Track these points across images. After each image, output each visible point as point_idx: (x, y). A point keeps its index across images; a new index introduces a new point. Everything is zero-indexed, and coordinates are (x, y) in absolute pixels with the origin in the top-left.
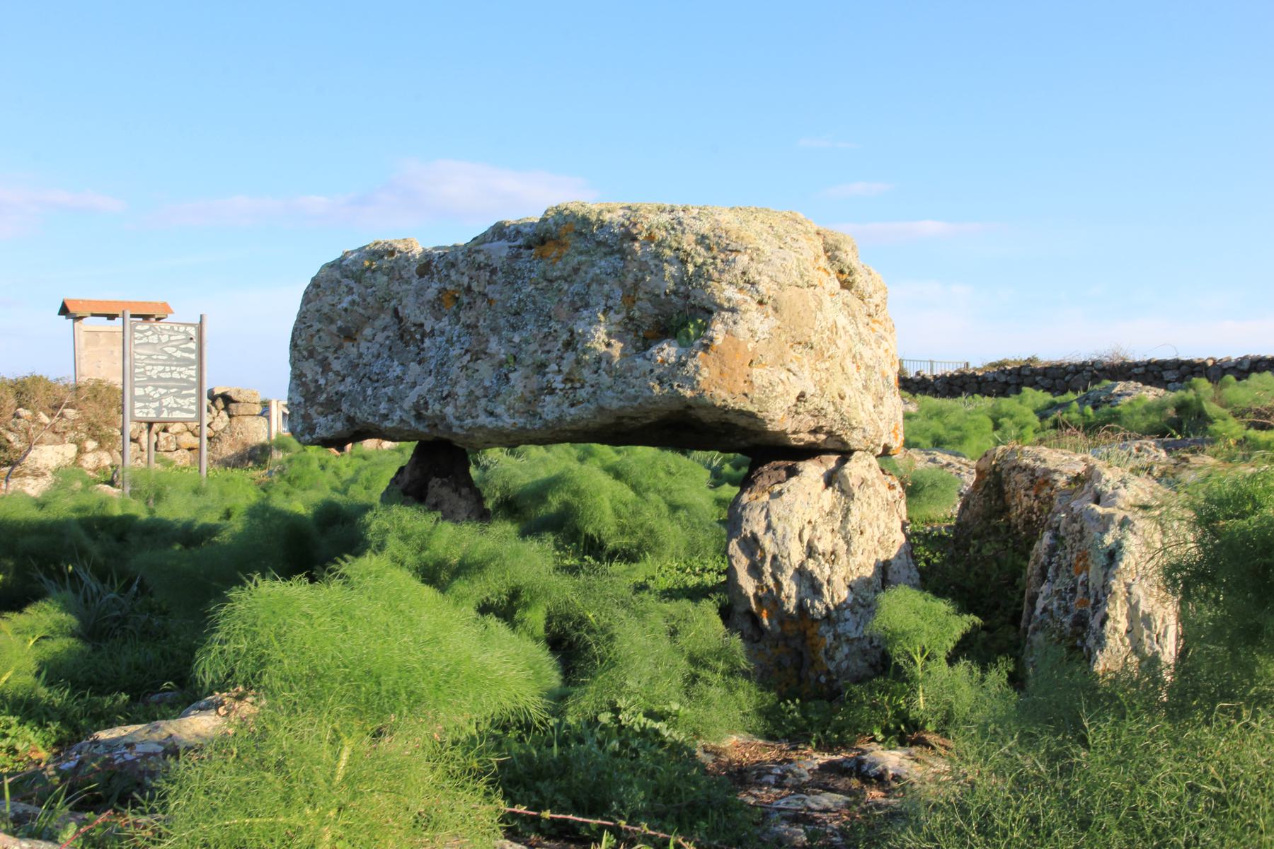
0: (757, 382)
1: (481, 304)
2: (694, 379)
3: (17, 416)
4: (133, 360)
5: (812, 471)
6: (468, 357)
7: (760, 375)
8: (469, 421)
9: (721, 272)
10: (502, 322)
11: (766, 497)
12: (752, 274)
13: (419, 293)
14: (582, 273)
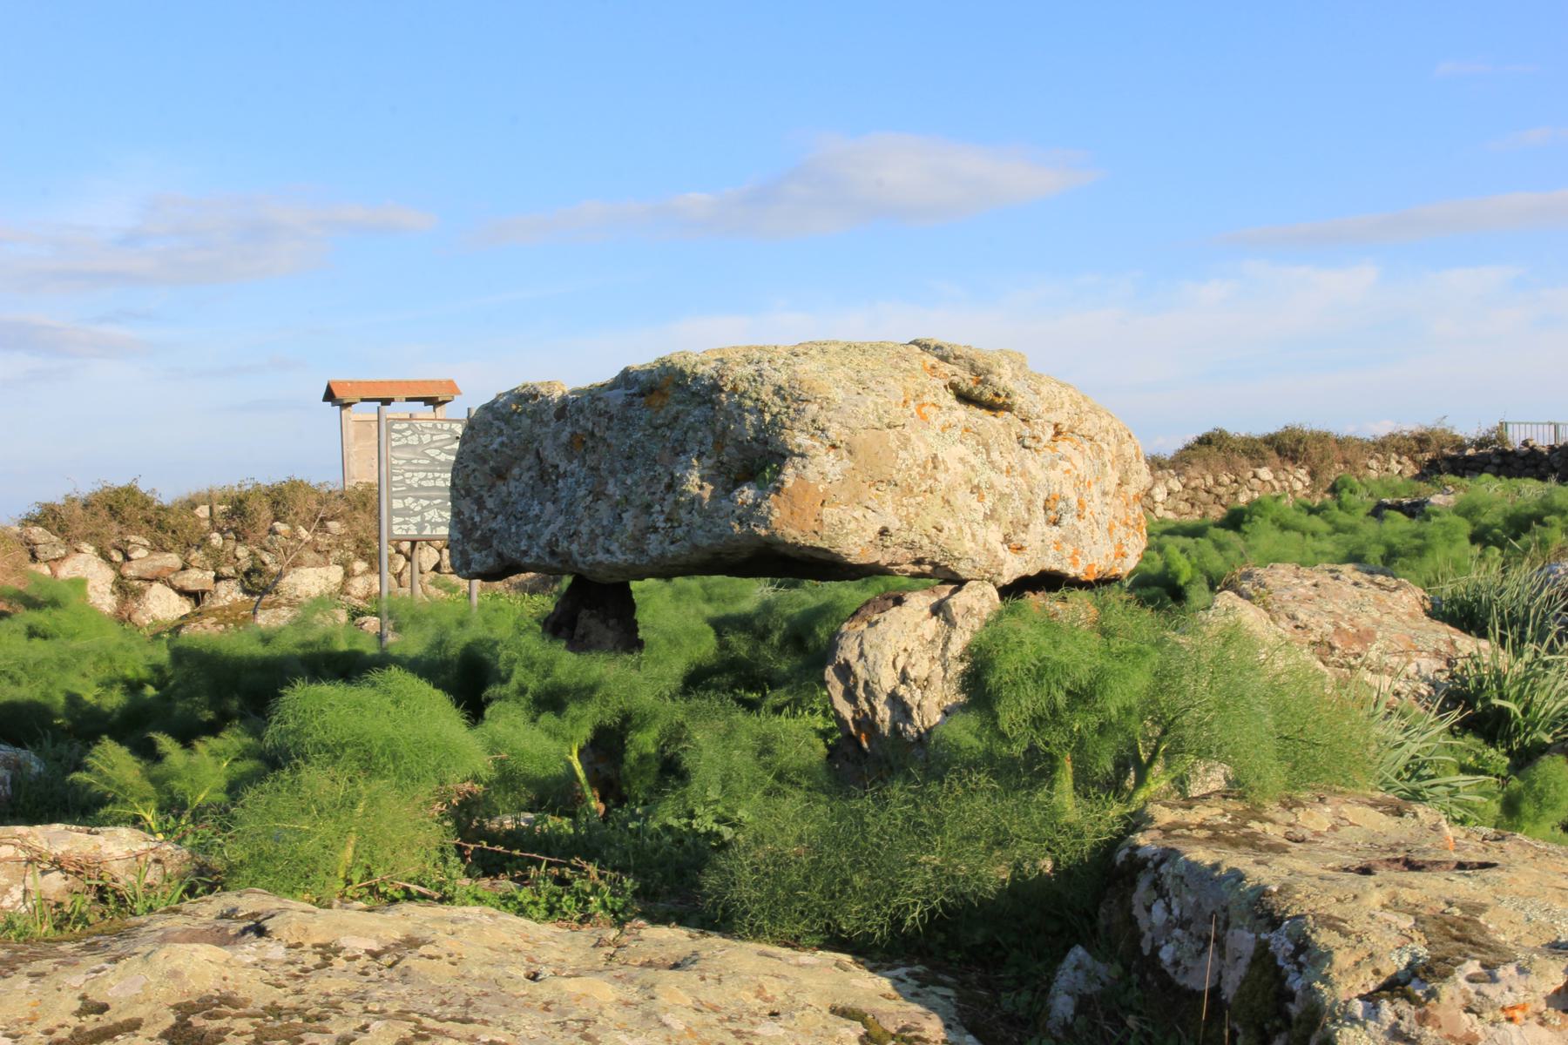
0: (827, 520)
1: (602, 449)
3: (272, 531)
4: (390, 466)
5: (919, 602)
6: (590, 498)
7: (830, 514)
8: (590, 558)
9: (793, 420)
10: (618, 465)
11: (865, 625)
12: (821, 421)
13: (556, 436)
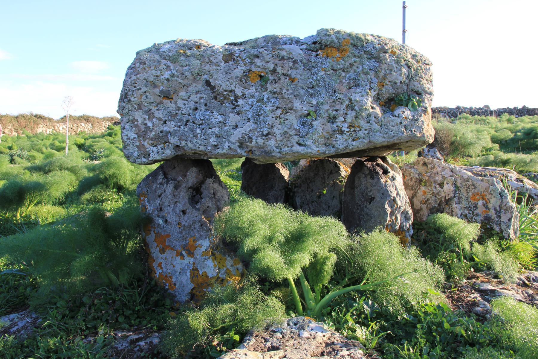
2: (421, 127)
14: (354, 68)
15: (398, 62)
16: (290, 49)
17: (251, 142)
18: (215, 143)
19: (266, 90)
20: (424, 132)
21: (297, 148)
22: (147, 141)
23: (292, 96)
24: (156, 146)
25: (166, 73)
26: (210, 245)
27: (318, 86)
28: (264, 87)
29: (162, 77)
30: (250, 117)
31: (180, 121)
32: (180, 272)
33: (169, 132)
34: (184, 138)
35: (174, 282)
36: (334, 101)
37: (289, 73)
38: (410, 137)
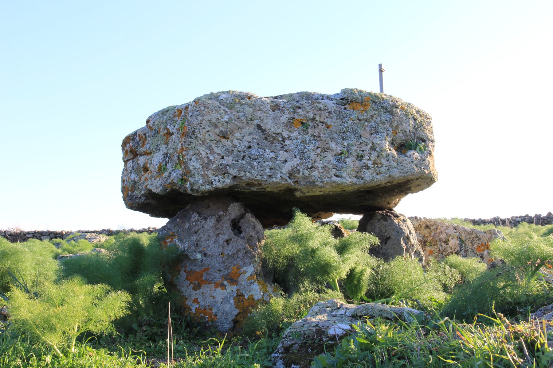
2: (428, 166)
14: (374, 119)
15: (407, 116)
16: (325, 103)
17: (299, 173)
18: (270, 174)
19: (308, 134)
20: (431, 170)
21: (335, 179)
22: (210, 171)
23: (328, 139)
24: (216, 176)
25: (225, 117)
26: (254, 271)
27: (348, 131)
28: (305, 131)
29: (222, 120)
30: (296, 154)
31: (237, 156)
32: (221, 302)
33: (228, 165)
34: (243, 169)
35: (214, 314)
36: (361, 144)
37: (325, 121)
38: (420, 173)
